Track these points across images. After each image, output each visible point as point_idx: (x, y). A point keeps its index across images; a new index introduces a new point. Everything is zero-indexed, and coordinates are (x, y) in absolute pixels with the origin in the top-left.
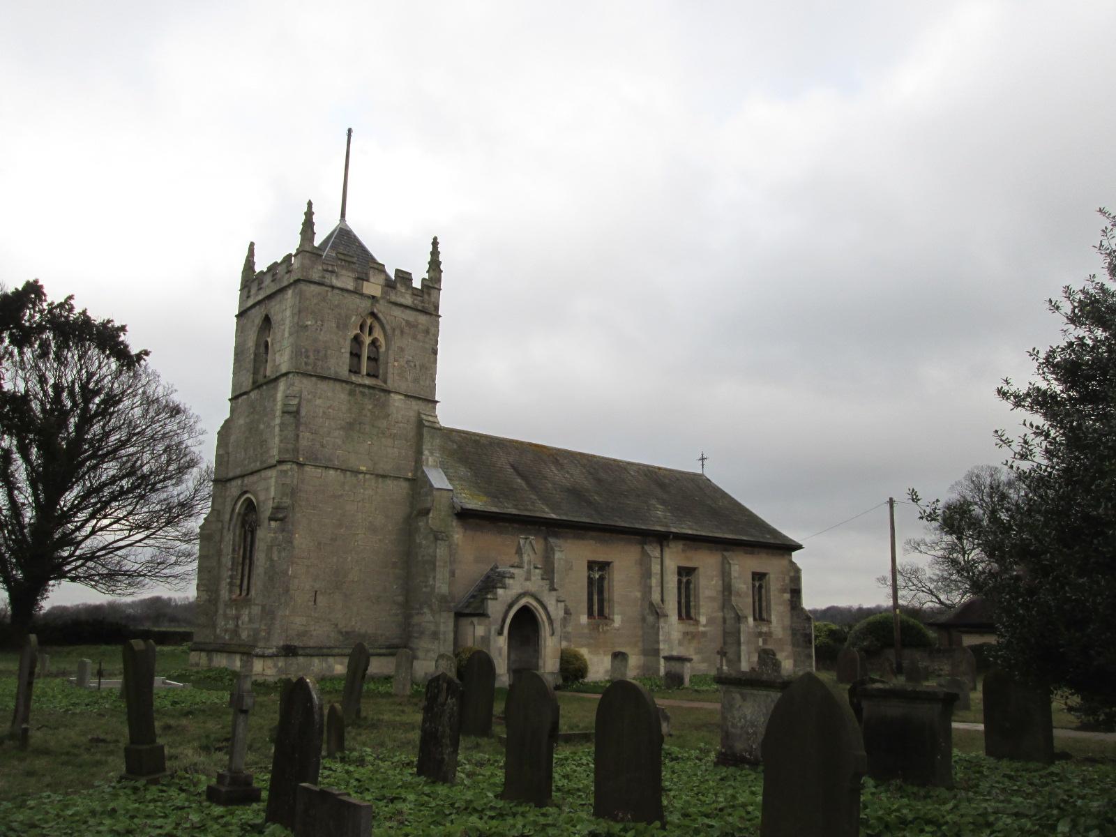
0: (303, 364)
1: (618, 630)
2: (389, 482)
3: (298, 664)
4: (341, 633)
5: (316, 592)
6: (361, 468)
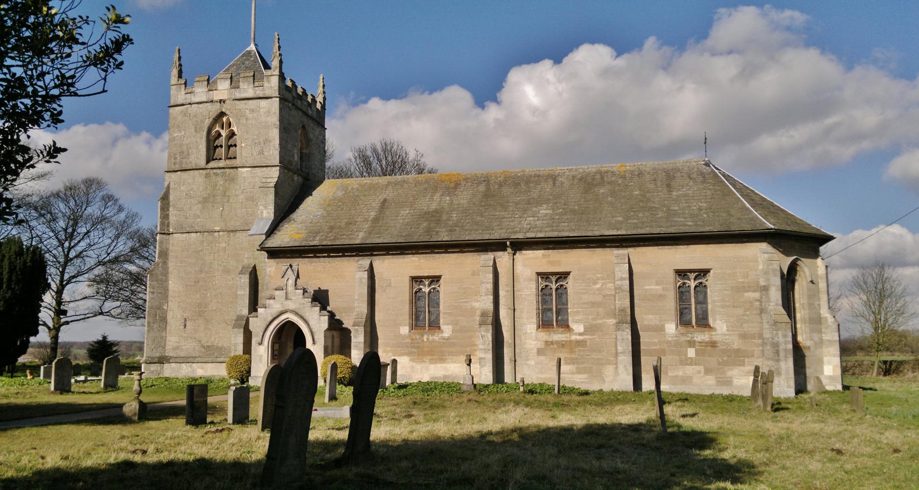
0: (173, 165)
1: (448, 339)
2: (238, 234)
3: (171, 368)
4: (204, 347)
5: (186, 319)
6: (216, 228)
